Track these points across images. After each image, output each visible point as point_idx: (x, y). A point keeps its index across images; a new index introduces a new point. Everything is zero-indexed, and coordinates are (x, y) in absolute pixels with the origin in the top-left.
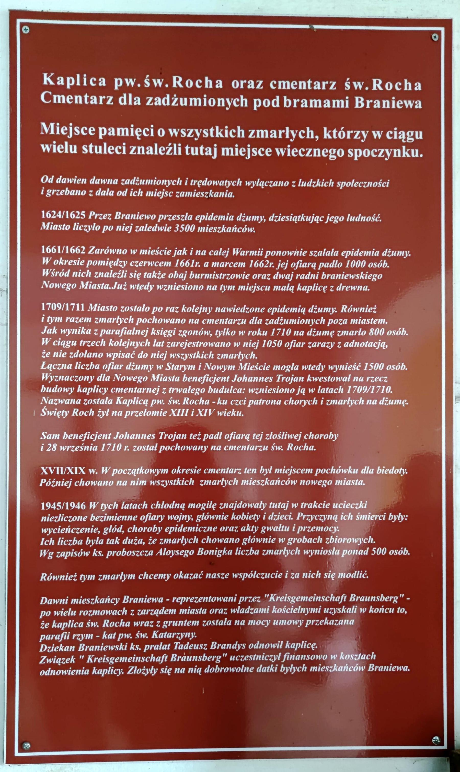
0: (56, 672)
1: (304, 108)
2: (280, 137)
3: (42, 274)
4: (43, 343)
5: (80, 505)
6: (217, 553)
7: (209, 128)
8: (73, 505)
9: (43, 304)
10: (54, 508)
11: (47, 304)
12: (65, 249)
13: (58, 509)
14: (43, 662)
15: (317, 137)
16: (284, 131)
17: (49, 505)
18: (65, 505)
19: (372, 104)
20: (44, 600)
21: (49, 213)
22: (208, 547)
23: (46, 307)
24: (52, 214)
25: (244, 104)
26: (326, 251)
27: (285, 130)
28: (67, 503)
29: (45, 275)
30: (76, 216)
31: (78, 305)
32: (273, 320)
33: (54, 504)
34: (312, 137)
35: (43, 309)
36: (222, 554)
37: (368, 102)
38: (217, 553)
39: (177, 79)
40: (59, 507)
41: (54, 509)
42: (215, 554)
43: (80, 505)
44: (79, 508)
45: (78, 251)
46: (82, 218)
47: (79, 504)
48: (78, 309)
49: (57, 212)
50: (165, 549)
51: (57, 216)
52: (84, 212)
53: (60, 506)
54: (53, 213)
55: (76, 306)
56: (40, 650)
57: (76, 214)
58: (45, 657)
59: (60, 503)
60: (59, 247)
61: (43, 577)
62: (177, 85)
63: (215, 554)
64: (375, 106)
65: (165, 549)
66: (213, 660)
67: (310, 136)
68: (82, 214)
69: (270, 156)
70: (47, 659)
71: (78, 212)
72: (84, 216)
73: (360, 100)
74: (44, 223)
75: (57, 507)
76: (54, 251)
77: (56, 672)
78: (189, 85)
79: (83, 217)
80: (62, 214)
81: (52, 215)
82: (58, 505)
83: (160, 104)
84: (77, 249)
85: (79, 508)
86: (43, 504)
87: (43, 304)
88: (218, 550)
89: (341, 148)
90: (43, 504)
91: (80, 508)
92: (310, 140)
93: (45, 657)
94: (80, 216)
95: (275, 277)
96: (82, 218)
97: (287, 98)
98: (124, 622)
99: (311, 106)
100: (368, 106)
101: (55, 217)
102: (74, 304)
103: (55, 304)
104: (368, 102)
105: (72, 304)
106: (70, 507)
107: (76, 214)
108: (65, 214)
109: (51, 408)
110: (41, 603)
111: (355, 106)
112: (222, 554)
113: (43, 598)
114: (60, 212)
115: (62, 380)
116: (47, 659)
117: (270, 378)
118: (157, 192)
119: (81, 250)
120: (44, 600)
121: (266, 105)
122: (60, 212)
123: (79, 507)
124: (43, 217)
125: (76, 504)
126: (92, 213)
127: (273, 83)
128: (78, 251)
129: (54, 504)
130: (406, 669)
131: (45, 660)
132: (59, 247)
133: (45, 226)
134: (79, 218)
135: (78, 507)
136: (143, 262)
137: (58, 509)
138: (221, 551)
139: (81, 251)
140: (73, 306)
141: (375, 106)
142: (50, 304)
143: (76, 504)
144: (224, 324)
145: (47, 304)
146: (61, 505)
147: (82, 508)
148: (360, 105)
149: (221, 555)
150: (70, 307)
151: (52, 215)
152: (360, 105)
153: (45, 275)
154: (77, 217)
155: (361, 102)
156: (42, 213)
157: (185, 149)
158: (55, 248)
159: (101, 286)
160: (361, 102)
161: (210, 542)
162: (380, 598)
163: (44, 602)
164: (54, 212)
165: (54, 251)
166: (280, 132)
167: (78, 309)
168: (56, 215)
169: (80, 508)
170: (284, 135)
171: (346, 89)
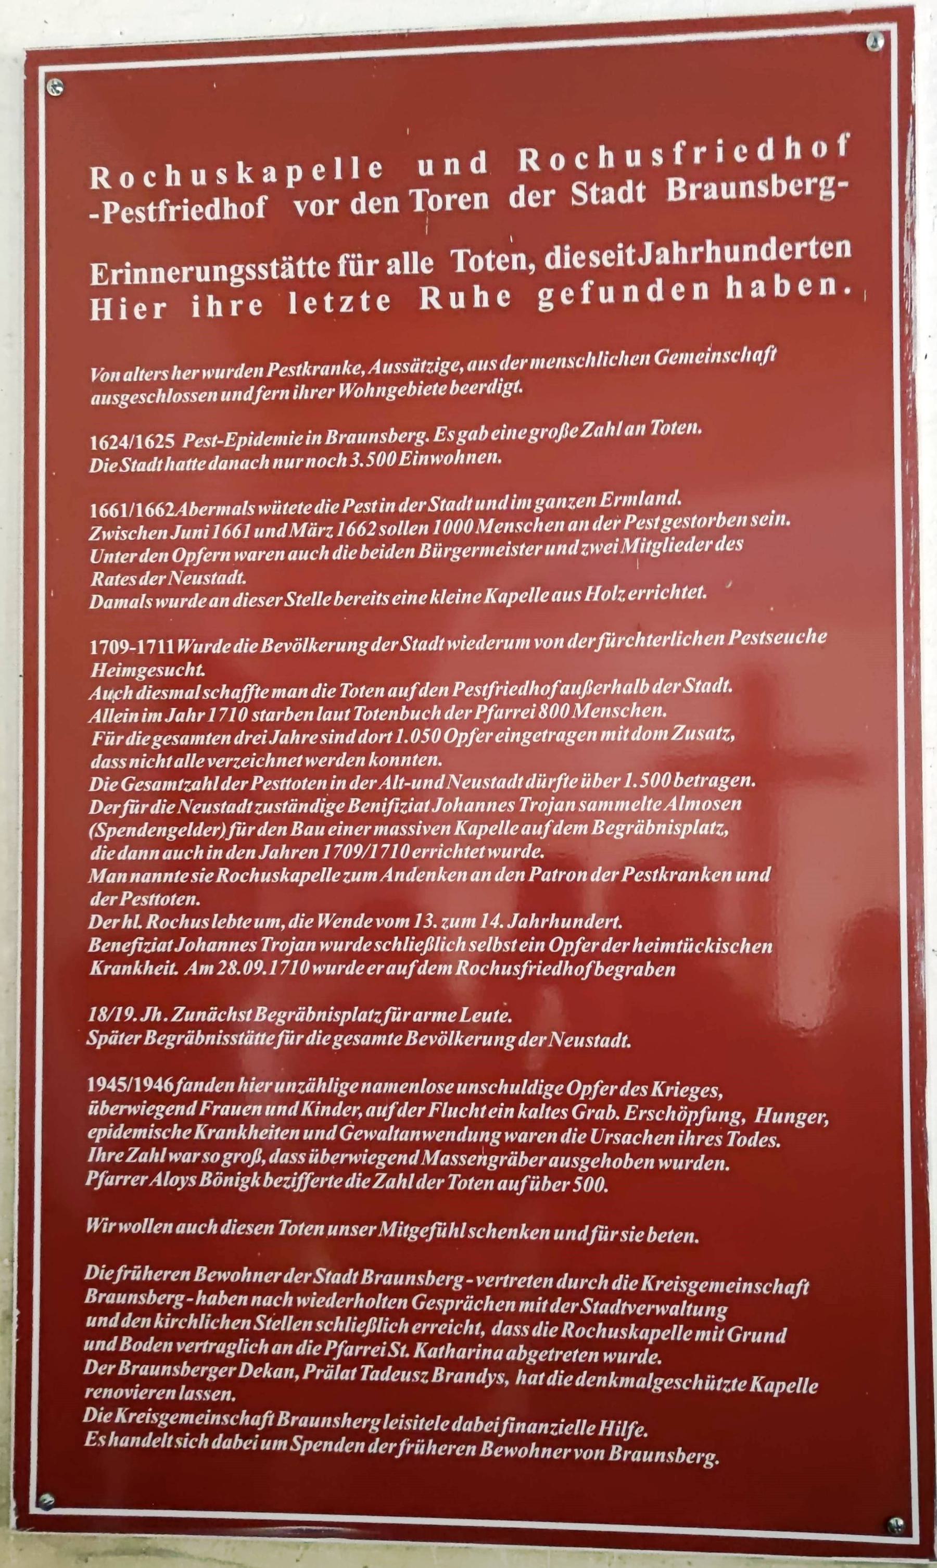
1: (711, 200)
2: (695, 260)
6: (240, 1183)
7: (269, 262)
8: (149, 1083)
10: (113, 1088)
15: (532, 267)
16: (701, 249)
17: (102, 1082)
18: (134, 1083)
19: (700, 193)
22: (278, 1170)
24: (111, 442)
25: (481, 204)
27: (705, 246)
28: (138, 1080)
34: (523, 267)
36: (249, 1184)
37: (693, 188)
38: (240, 1183)
39: (100, 173)
40: (121, 1087)
42: (236, 1185)
47: (160, 1080)
49: (120, 439)
50: (168, 1173)
53: (124, 1085)
57: (156, 440)
62: (528, 166)
63: (236, 1185)
64: (706, 196)
65: (168, 1173)
66: (698, 1461)
67: (680, 259)
68: (168, 440)
69: (808, 297)
71: (161, 436)
73: (677, 184)
75: (119, 1087)
78: (557, 160)
79: (169, 444)
80: (129, 442)
81: (110, 444)
82: (120, 1083)
83: (612, 201)
86: (91, 1080)
88: (241, 1176)
92: (519, 271)
94: (164, 443)
97: (778, 178)
99: (743, 195)
100: (693, 197)
104: (693, 188)
106: (143, 1087)
107: (111, 442)
108: (136, 440)
111: (667, 196)
112: (249, 1184)
114: (125, 438)
118: (424, 386)
121: (317, 211)
122: (125, 438)
124: (94, 448)
125: (155, 1081)
126: (189, 437)
127: (581, 157)
129: (113, 1079)
135: (160, 1088)
138: (248, 1179)
141: (706, 196)
143: (155, 1081)
146: (127, 1082)
148: (677, 194)
149: (247, 1188)
151: (110, 444)
152: (677, 194)
154: (159, 446)
155: (679, 189)
156: (91, 441)
157: (323, 301)
160: (679, 189)
161: (608, 1166)
162: (425, 1279)
164: (115, 437)
166: (695, 251)
168: (117, 444)
170: (702, 256)
171: (654, 163)
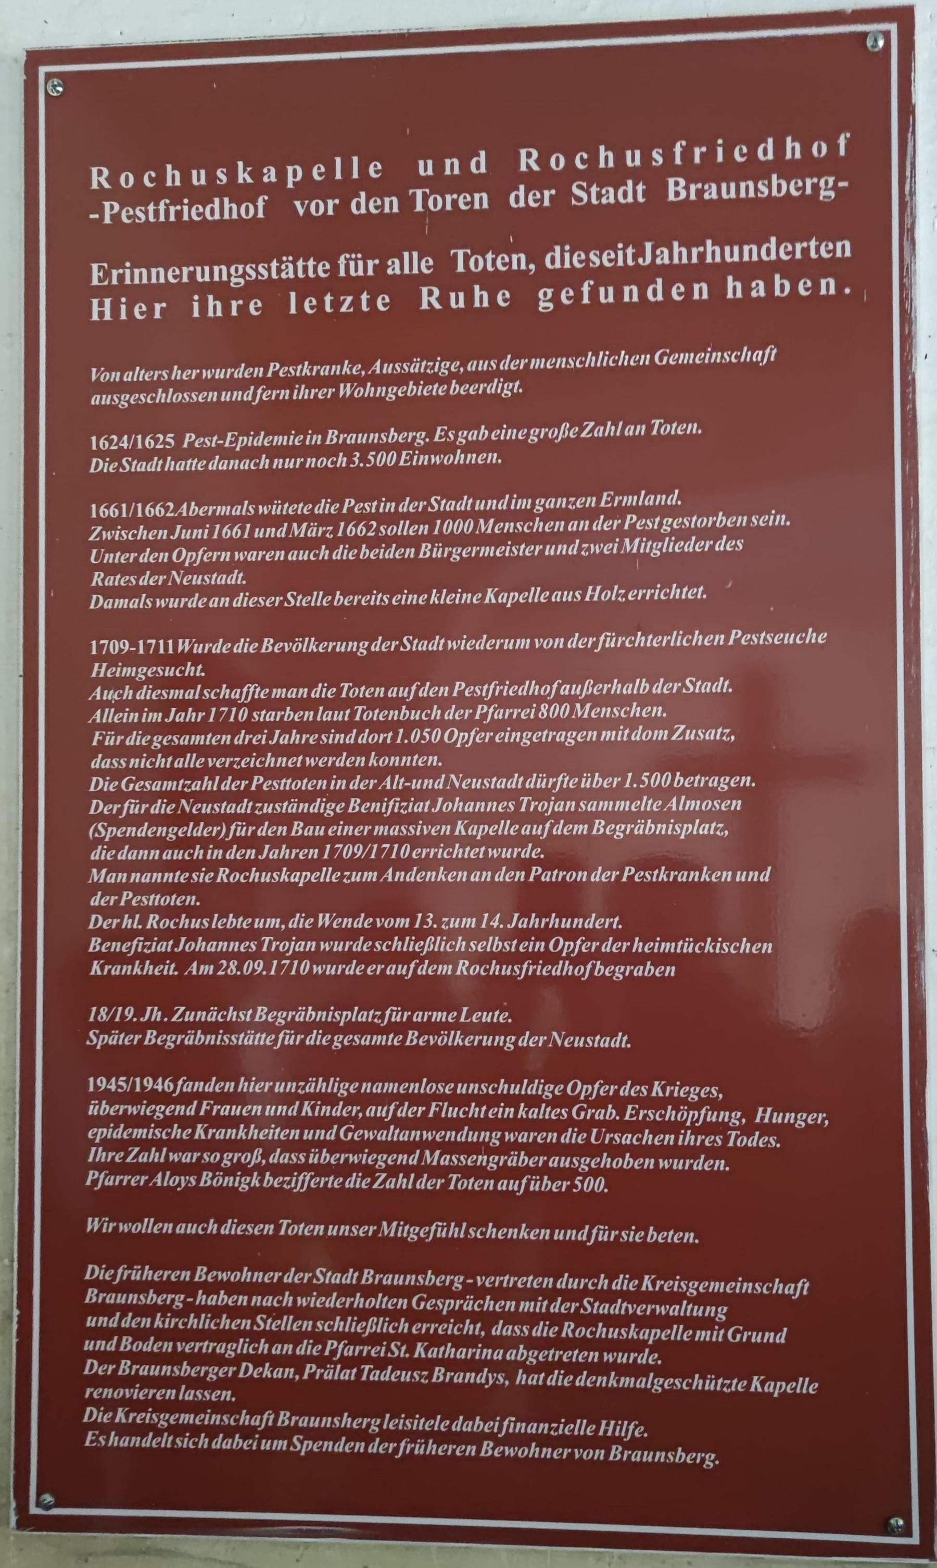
0: (114, 1392)
3: (86, 1227)
4: (89, 1228)
5: (163, 1084)
8: (149, 1083)
9: (94, 643)
10: (113, 1088)
11: (102, 642)
12: (136, 508)
13: (120, 1090)
14: (96, 537)
17: (102, 1082)
18: (134, 1083)
20: (98, 600)
21: (105, 439)
23: (100, 647)
24: (111, 442)
26: (700, 825)
28: (138, 1080)
29: (92, 1229)
30: (156, 444)
31: (161, 642)
32: (608, 1039)
33: (113, 1080)
35: (94, 652)
40: (122, 1087)
41: (113, 1090)
43: (163, 1084)
44: (160, 1090)
45: (160, 511)
46: (167, 447)
47: (160, 1080)
48: (162, 651)
49: (120, 439)
51: (121, 445)
52: (172, 435)
54: (113, 440)
55: (157, 645)
56: (84, 1371)
57: (156, 440)
58: (100, 528)
59: (124, 1078)
60: (124, 506)
61: (93, 1224)
68: (168, 440)
70: (104, 533)
71: (161, 436)
72: (172, 442)
74: (94, 871)
76: (114, 514)
77: (114, 1392)
79: (169, 444)
80: (129, 442)
82: (120, 1083)
84: (158, 508)
85: (160, 1090)
86: (91, 1080)
87: (94, 643)
89: (554, 171)
90: (91, 1080)
91: (163, 1089)
93: (100, 528)
94: (164, 443)
95: (595, 877)
96: (167, 447)
98: (248, 1417)
101: (116, 448)
102: (154, 641)
103: (116, 642)
105: (149, 641)
106: (143, 1087)
108: (136, 440)
109: (109, 593)
110: (86, 1372)
113: (90, 1267)
115: (133, 835)
116: (104, 533)
117: (510, 804)
119: (167, 509)
120: (98, 600)
122: (125, 437)
123: (160, 1088)
124: (94, 448)
125: (155, 1081)
126: (189, 437)
128: (160, 511)
129: (113, 1080)
130: (690, 1237)
131: (100, 534)
132: (124, 506)
133: (97, 602)
134: (162, 447)
136: (367, 1228)
137: (120, 1090)
139: (166, 512)
140: (151, 644)
142: (106, 642)
143: (155, 1081)
144: (463, 858)
145: (102, 642)
146: (127, 1082)
147: (166, 1089)
150: (147, 647)
153: (92, 1229)
154: (159, 447)
158: (115, 507)
159: (220, 808)
163: (91, 1370)
164: (115, 437)
165: (114, 514)
167: (162, 651)
168: (117, 444)
169: (163, 1089)
